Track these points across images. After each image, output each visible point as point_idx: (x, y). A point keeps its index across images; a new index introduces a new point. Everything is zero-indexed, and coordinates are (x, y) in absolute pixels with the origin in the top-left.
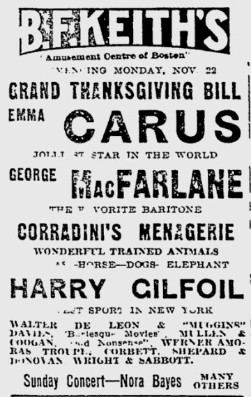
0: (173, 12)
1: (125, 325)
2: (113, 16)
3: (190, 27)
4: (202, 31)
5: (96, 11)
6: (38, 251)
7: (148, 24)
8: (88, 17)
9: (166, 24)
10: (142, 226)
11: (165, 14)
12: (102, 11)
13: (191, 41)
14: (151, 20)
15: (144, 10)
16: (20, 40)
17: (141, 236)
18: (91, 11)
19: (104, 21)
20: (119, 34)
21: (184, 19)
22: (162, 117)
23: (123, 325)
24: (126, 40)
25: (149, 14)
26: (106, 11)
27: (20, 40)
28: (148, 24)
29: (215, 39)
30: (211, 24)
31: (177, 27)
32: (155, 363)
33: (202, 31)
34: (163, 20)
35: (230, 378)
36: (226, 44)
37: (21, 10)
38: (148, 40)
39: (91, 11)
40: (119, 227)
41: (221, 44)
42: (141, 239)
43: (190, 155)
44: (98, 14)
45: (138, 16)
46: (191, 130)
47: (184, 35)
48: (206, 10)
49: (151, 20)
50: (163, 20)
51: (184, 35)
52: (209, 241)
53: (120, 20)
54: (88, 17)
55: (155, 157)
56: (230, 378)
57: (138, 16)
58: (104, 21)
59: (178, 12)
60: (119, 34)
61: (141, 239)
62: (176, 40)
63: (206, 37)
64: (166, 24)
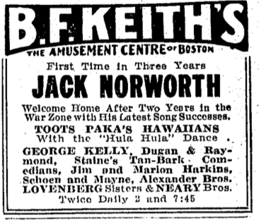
0: (186, 7)
1: (42, 152)
2: (120, 13)
3: (205, 20)
5: (101, 9)
7: (157, 19)
8: (93, 14)
9: (179, 19)
11: (177, 9)
12: (109, 8)
13: (207, 34)
15: (153, 6)
17: (102, 92)
18: (95, 8)
19: (110, 20)
20: (128, 29)
21: (197, 12)
22: (157, 46)
23: (39, 151)
24: (133, 35)
25: (159, 9)
26: (113, 8)
28: (157, 19)
29: (232, 31)
34: (175, 14)
37: (7, 7)
39: (95, 8)
40: (72, 171)
41: (237, 38)
42: (102, 96)
43: (221, 189)
44: (104, 11)
45: (147, 13)
47: (198, 29)
49: (161, 15)
50: (175, 14)
51: (198, 29)
52: (191, 62)
53: (128, 16)
54: (93, 14)
55: (144, 69)
58: (110, 20)
59: (191, 7)
60: (128, 29)
61: (102, 96)
62: (189, 34)
63: (223, 32)
64: (179, 19)
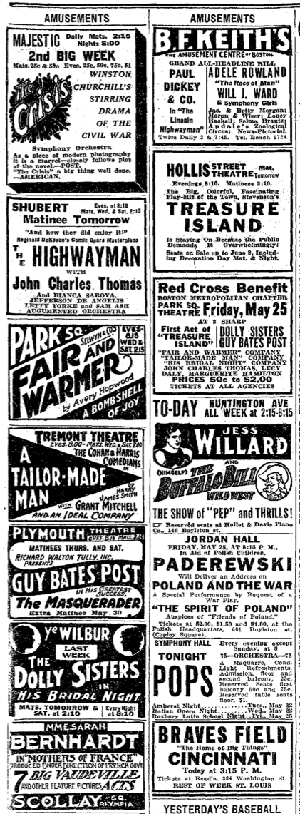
4: (276, 41)
6: (109, 148)
7: (240, 38)
9: (252, 37)
10: (168, 165)
11: (252, 32)
13: (269, 46)
14: (242, 34)
16: (12, 4)
20: (223, 43)
21: (263, 34)
24: (226, 46)
25: (241, 32)
27: (12, 4)
28: (240, 38)
29: (283, 44)
30: (281, 36)
31: (259, 38)
32: (168, 252)
33: (276, 41)
35: (215, 610)
36: (12, 548)
38: (240, 46)
41: (286, 48)
45: (234, 33)
46: (32, 209)
47: (264, 43)
48: (279, 29)
49: (242, 34)
50: (250, 35)
56: (215, 610)
57: (234, 33)
58: (213, 37)
62: (259, 46)
64: (252, 37)
